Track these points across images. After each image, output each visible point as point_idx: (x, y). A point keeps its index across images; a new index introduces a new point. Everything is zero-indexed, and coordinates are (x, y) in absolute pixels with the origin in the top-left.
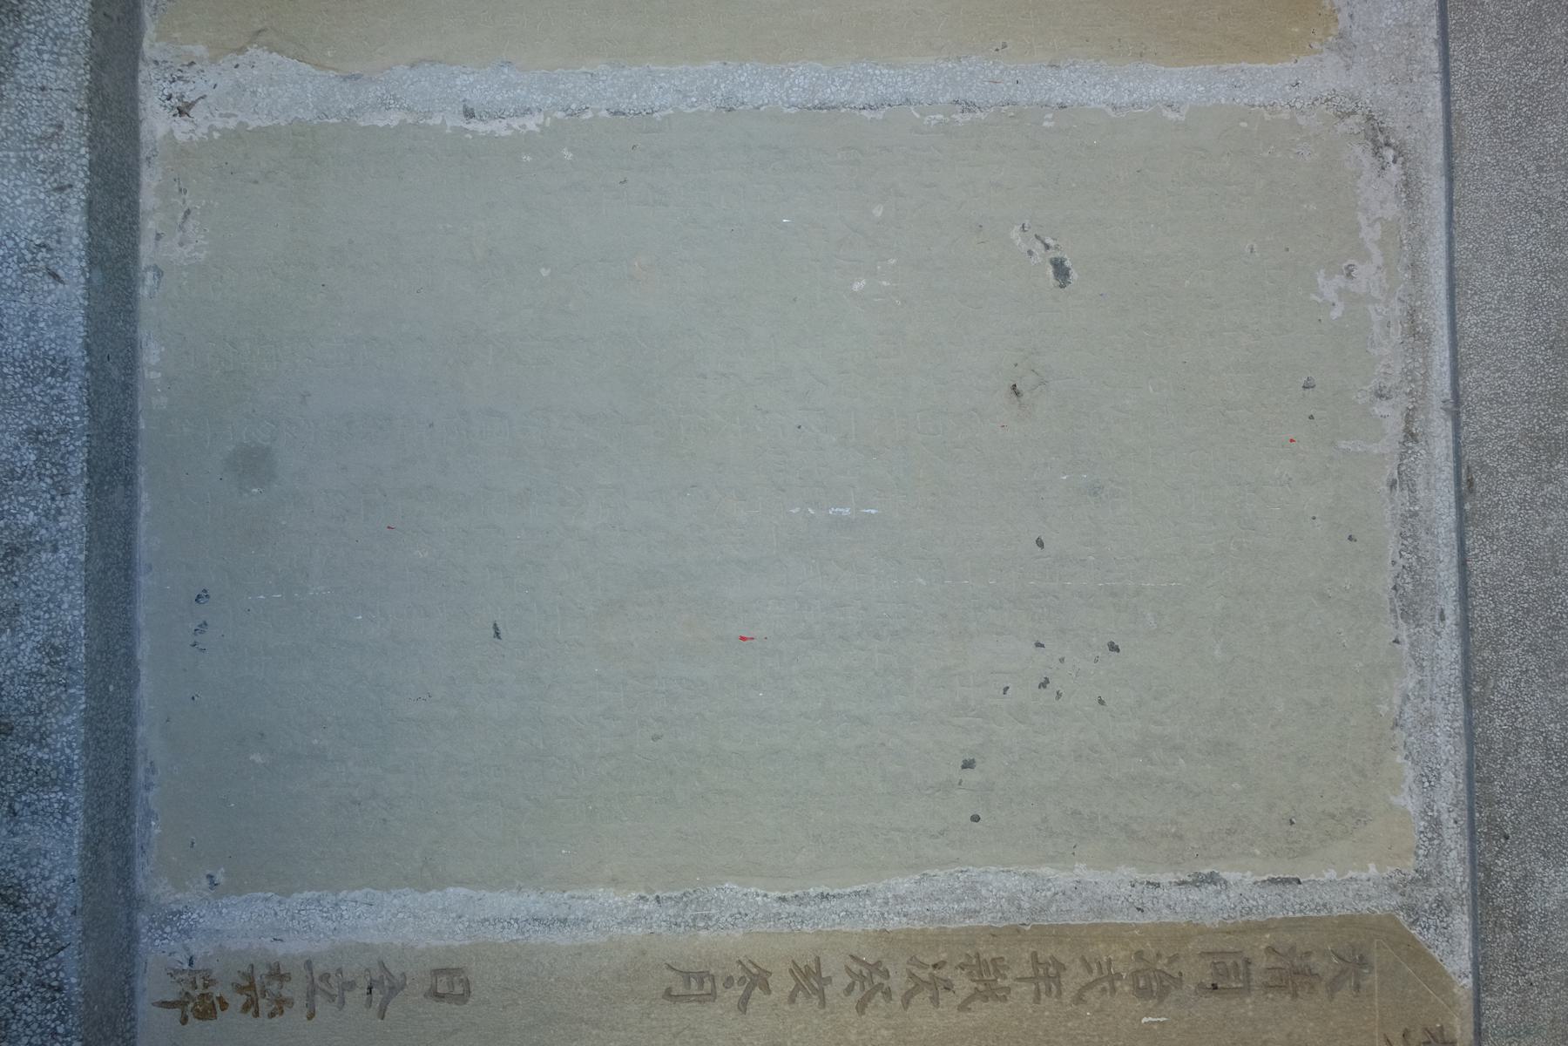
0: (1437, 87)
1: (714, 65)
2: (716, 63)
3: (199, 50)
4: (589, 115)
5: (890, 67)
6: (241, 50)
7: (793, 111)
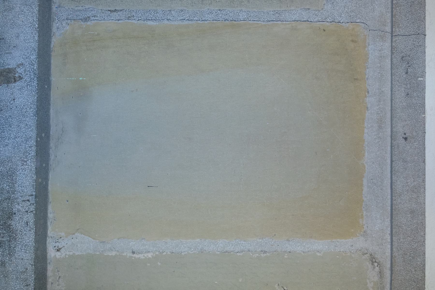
0: (389, 246)
1: (198, 240)
2: (199, 239)
3: (63, 234)
4: (165, 254)
5: (244, 241)
6: (74, 234)
7: (218, 253)
